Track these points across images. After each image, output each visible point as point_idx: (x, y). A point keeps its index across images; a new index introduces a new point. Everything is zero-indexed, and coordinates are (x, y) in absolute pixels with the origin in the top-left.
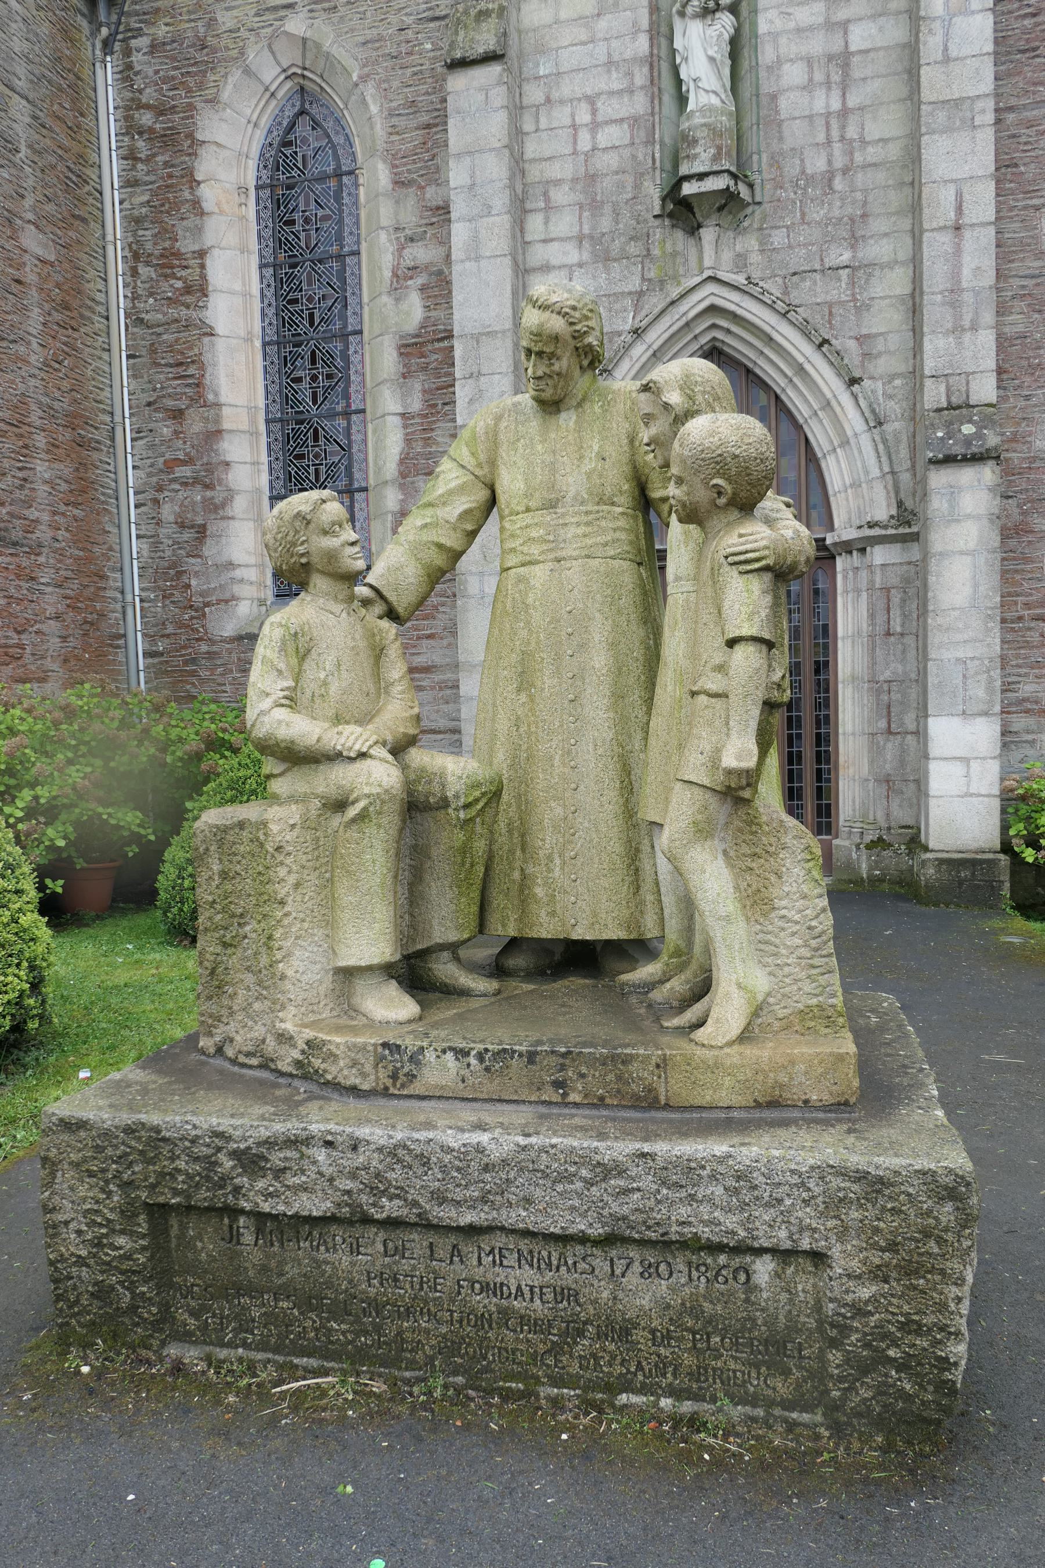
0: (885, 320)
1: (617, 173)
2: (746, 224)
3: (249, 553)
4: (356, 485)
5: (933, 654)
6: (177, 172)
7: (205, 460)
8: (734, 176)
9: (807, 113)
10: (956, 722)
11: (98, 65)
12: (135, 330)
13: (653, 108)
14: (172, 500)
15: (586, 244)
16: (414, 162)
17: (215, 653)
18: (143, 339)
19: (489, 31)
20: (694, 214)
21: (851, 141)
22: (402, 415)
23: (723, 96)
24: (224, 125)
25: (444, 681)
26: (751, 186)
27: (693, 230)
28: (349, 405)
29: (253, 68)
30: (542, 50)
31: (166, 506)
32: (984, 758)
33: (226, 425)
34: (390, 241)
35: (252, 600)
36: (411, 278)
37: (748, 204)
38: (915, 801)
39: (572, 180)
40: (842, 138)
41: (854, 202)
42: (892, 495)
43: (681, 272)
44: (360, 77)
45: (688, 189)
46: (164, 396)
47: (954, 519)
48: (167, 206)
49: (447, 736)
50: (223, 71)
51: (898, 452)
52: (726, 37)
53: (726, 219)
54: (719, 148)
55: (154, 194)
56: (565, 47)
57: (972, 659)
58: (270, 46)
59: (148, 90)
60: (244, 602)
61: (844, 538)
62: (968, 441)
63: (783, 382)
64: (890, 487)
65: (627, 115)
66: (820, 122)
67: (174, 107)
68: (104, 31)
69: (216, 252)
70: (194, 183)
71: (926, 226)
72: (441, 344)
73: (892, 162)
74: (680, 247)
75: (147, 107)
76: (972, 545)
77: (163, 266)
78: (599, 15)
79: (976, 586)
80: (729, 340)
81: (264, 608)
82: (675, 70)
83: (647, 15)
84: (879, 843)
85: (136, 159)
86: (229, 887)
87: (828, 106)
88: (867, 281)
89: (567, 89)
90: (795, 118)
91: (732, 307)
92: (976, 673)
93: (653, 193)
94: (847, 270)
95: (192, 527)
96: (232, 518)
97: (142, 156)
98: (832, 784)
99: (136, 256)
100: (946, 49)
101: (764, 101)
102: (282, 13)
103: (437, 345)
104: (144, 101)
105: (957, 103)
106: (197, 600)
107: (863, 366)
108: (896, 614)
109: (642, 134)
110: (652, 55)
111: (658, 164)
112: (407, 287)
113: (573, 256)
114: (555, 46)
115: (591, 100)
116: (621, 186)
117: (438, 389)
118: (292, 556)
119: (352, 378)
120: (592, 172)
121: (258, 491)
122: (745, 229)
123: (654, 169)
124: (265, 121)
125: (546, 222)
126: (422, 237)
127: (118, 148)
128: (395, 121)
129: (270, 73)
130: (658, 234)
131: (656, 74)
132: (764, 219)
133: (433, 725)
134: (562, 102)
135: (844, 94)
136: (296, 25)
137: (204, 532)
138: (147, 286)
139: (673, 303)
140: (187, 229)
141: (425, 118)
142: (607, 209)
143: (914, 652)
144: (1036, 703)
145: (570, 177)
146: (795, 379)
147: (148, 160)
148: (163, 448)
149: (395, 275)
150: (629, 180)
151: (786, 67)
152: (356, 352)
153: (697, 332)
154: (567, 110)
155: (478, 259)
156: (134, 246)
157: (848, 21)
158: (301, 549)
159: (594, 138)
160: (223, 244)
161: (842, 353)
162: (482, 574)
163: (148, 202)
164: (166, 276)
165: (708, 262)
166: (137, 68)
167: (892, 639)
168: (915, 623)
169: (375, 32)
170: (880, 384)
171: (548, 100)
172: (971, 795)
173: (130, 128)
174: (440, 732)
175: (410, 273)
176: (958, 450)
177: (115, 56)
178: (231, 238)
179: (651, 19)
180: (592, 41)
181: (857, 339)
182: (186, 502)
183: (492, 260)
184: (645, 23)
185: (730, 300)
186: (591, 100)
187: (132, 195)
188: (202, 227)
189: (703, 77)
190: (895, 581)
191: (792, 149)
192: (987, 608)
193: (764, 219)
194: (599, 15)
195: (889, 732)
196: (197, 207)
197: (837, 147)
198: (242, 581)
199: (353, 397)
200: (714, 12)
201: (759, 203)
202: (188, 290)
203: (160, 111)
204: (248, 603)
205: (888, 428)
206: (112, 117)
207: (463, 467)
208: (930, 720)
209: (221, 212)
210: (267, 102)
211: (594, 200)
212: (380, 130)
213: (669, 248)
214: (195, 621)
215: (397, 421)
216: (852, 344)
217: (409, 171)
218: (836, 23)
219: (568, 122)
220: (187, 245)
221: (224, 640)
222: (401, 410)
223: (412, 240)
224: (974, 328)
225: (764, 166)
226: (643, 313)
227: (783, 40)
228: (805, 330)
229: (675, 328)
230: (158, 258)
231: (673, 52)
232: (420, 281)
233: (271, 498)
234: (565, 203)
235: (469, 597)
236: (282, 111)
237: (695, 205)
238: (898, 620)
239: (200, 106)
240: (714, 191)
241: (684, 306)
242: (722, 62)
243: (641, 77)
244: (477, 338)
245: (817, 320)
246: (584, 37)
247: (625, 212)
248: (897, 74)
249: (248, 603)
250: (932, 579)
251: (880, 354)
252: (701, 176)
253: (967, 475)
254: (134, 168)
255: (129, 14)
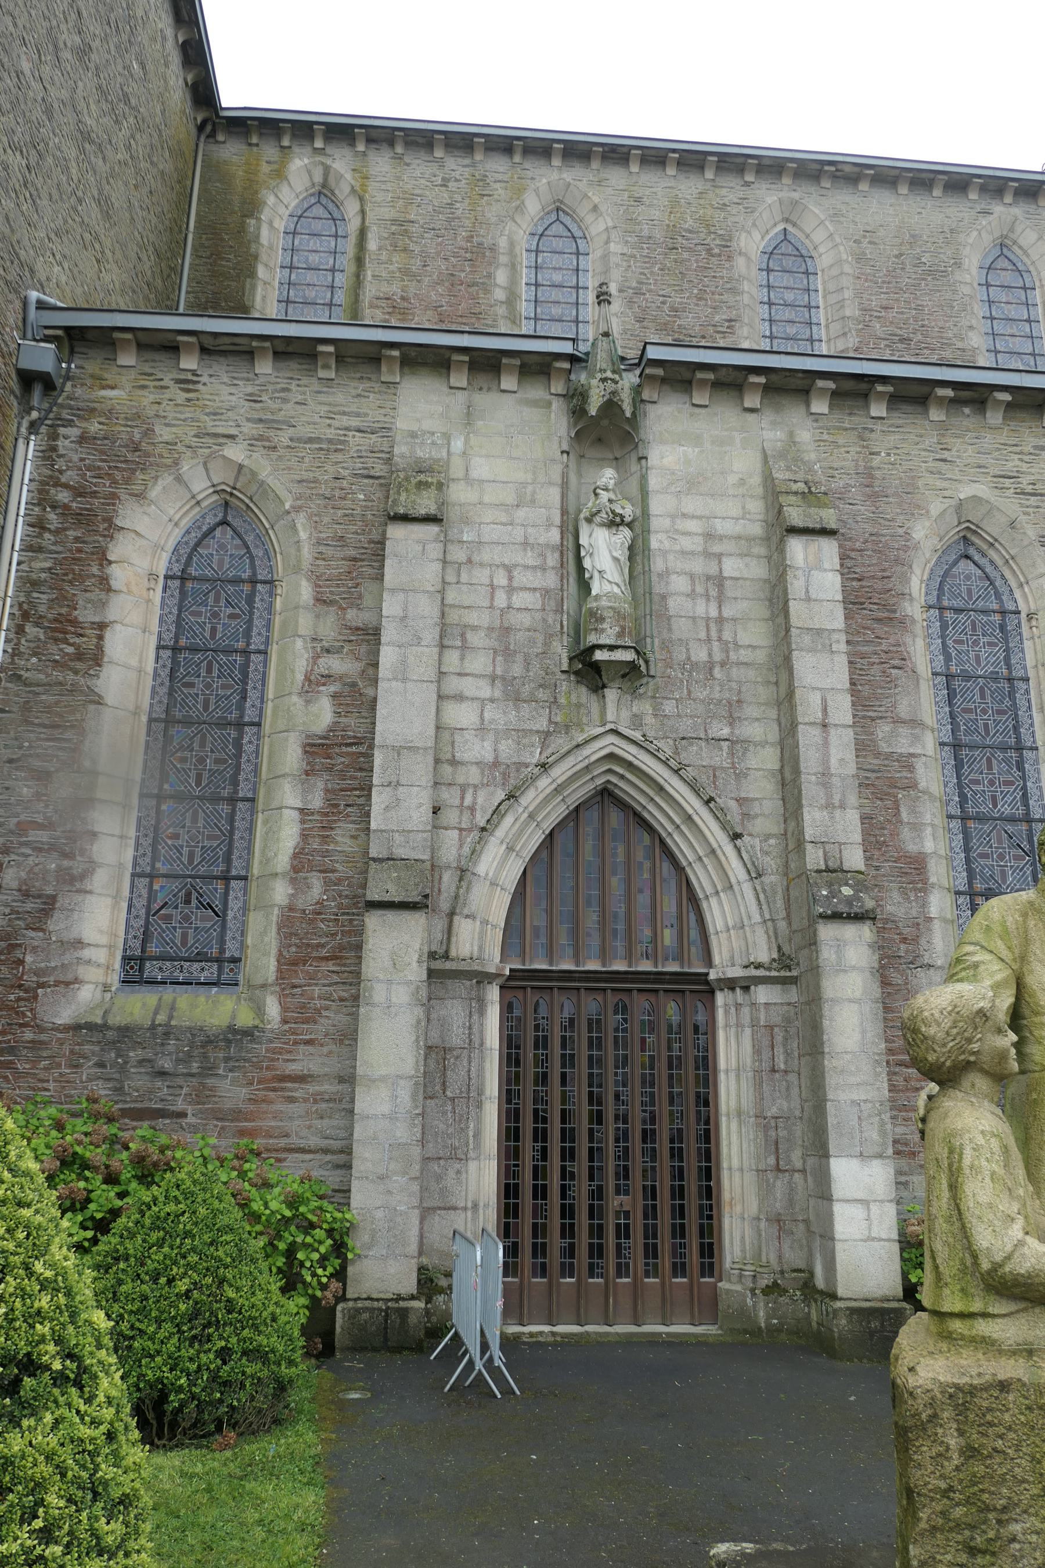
0: (761, 789)
1: (529, 630)
2: (641, 691)
3: (101, 932)
4: (234, 873)
5: (830, 1095)
6: (88, 548)
7: (68, 827)
8: (638, 652)
10: (854, 1164)
11: (21, 441)
12: (9, 685)
14: (19, 865)
16: (338, 586)
17: (41, 1042)
18: (18, 696)
19: (429, 498)
20: (600, 677)
21: (727, 643)
22: (301, 810)
24: (146, 518)
25: (320, 1093)
26: (647, 662)
27: (598, 688)
28: (236, 792)
29: (185, 478)
30: (466, 521)
31: (11, 871)
32: (882, 1201)
33: (100, 794)
34: (305, 648)
35: (97, 984)
36: (324, 685)
38: (804, 1242)
41: (730, 690)
42: (773, 939)
43: (585, 720)
44: (292, 507)
45: (599, 655)
46: (31, 756)
47: (842, 969)
48: (70, 576)
49: (318, 1156)
50: (153, 474)
51: (775, 902)
54: (623, 628)
55: (58, 562)
57: (865, 1101)
58: (205, 464)
59: (69, 473)
60: (87, 987)
61: (730, 975)
62: (849, 901)
63: (670, 828)
64: (771, 933)
66: (702, 624)
67: (95, 492)
68: (35, 415)
69: (118, 627)
70: (104, 560)
71: (800, 720)
72: (349, 749)
74: (584, 700)
75: (66, 486)
76: (858, 994)
77: (55, 630)
79: (863, 1032)
81: (108, 995)
82: (579, 560)
83: (559, 516)
84: (773, 1289)
85: (43, 528)
86: (980, 1469)
87: (707, 612)
88: (744, 754)
89: (486, 555)
91: (630, 758)
92: (870, 1116)
93: (561, 652)
95: (39, 896)
96: (90, 892)
97: (52, 527)
98: (715, 1222)
99: (25, 615)
100: (807, 591)
101: (656, 598)
102: (222, 440)
103: (344, 749)
104: (63, 480)
105: (819, 632)
106: (30, 980)
108: (779, 1050)
109: (553, 603)
112: (318, 692)
113: (486, 692)
115: (509, 569)
116: (532, 642)
117: (342, 790)
118: (963, 1053)
119: (243, 766)
121: (121, 866)
123: (562, 633)
124: (185, 523)
125: (462, 658)
126: (339, 650)
127: (26, 515)
128: (322, 548)
129: (200, 485)
132: (657, 689)
133: (302, 1143)
134: (481, 565)
136: (236, 453)
137: (53, 904)
138: (32, 645)
139: (578, 746)
140: (89, 601)
141: (352, 552)
142: (519, 658)
143: (797, 1090)
144: (906, 1145)
146: (682, 827)
147: (57, 532)
148: (19, 809)
149: (307, 679)
150: (540, 638)
151: (674, 577)
152: (250, 742)
154: (487, 572)
155: (404, 680)
156: (25, 606)
158: (975, 1047)
160: (127, 621)
162: (389, 982)
163: (50, 569)
164: (56, 640)
165: (610, 717)
166: (61, 451)
167: (777, 1075)
168: (796, 1061)
169: (311, 475)
170: (757, 841)
171: (470, 561)
172: (873, 1239)
173: (42, 498)
174: (310, 1152)
175: (323, 680)
176: (843, 908)
177: (40, 437)
178: (135, 617)
182: (36, 870)
184: (557, 520)
185: (629, 752)
186: (509, 569)
187: (32, 559)
188: (107, 601)
190: (777, 1020)
192: (875, 1054)
193: (657, 689)
195: (778, 1169)
196: (105, 584)
197: (716, 644)
198: (89, 962)
199: (242, 785)
202: (79, 656)
203: (79, 492)
204: (92, 987)
205: (767, 880)
206: (25, 488)
207: (1002, 960)
208: (832, 1161)
209: (129, 592)
210: (191, 508)
211: (507, 648)
212: (307, 553)
214: (22, 1003)
215: (295, 815)
216: (733, 804)
217: (331, 593)
219: (487, 581)
220: (86, 615)
221: (57, 1028)
222: (300, 806)
223: (328, 651)
224: (843, 806)
225: (656, 648)
226: (550, 751)
227: (671, 557)
228: (694, 787)
229: (575, 770)
230: (50, 622)
231: (578, 547)
232: (332, 689)
233: (133, 875)
235: (373, 1005)
236: (203, 517)
237: (603, 669)
238: (782, 1057)
239: (123, 497)
241: (587, 751)
244: (398, 750)
245: (703, 779)
246: (504, 520)
247: (536, 664)
249: (92, 987)
250: (826, 1023)
251: (756, 816)
252: (612, 648)
253: (850, 931)
254: (40, 536)
255: (62, 406)
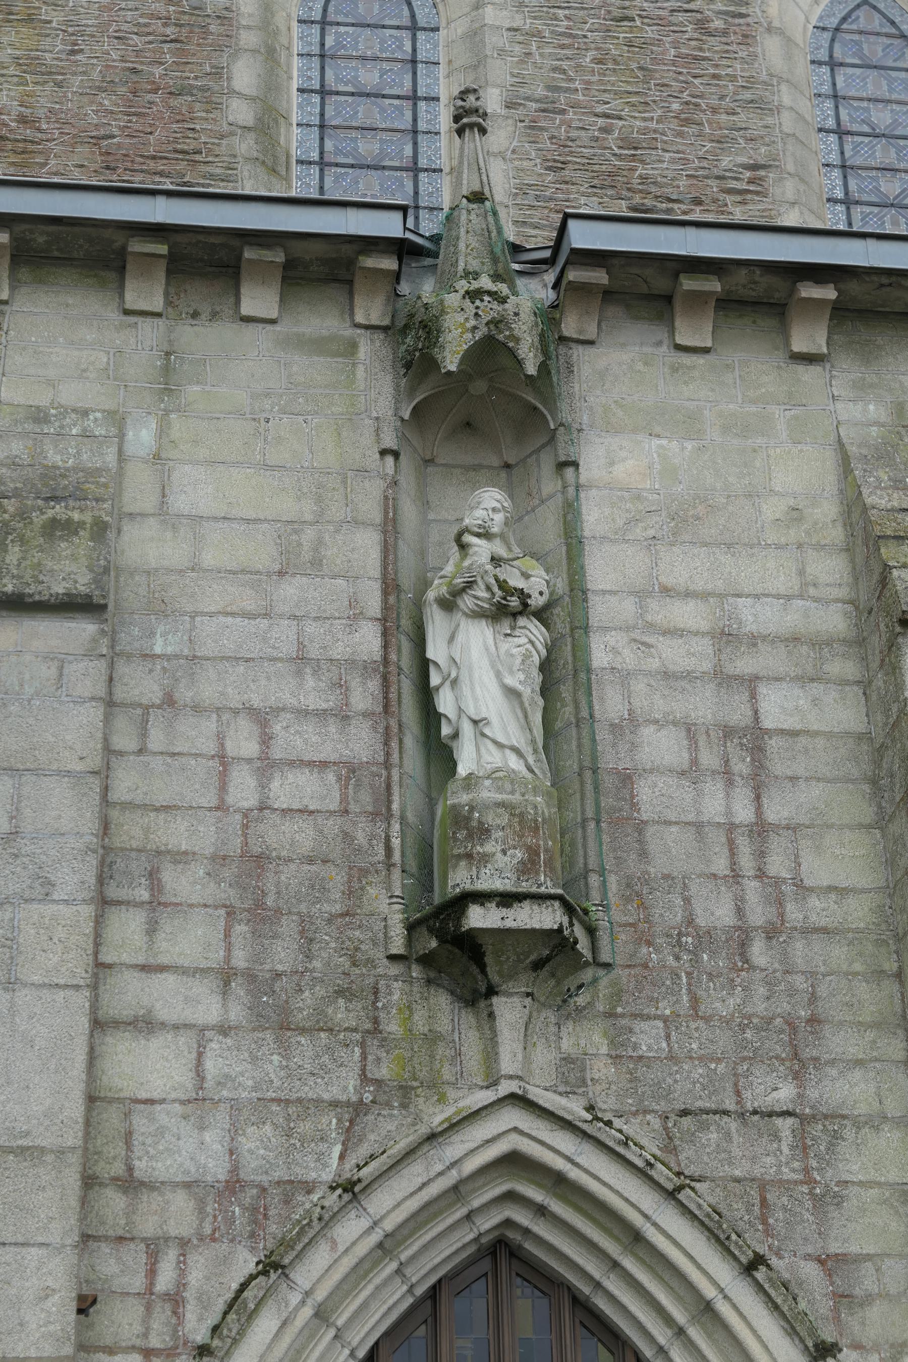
1: (311, 861)
8: (569, 909)
9: (691, 817)
13: (388, 754)
15: (238, 988)
19: (74, 558)
20: (483, 968)
21: (778, 882)
23: (531, 760)
26: (591, 931)
27: (477, 996)
30: (161, 608)
37: (587, 964)
39: (213, 858)
40: (761, 874)
41: (792, 992)
43: (447, 1073)
45: (478, 918)
52: (536, 660)
53: (545, 986)
54: (533, 852)
56: (211, 615)
63: (662, 1335)
65: (333, 757)
73: (857, 931)
74: (444, 1024)
78: (281, 573)
80: (541, 1229)
82: (426, 695)
87: (729, 812)
90: (669, 823)
93: (387, 911)
94: (790, 1121)
101: (608, 782)
107: (837, 1319)
109: (366, 797)
110: (386, 661)
111: (397, 857)
113: (208, 1008)
114: (189, 608)
115: (262, 719)
116: (319, 887)
120: (257, 850)
122: (579, 1010)
123: (389, 866)
125: (152, 929)
130: (397, 993)
131: (393, 696)
132: (617, 995)
134: (197, 709)
135: (758, 797)
139: (432, 1137)
142: (288, 926)
145: (208, 851)
146: (693, 1332)
150: (337, 879)
151: (647, 731)
153: (476, 1204)
154: (210, 725)
157: (756, 678)
159: (263, 787)
161: (793, 1286)
165: (508, 1063)
171: (169, 701)
179: (385, 601)
180: (266, 615)
181: (821, 1262)
183: (45, 993)
184: (373, 604)
185: (557, 1149)
186: (262, 719)
189: (495, 720)
191: (666, 877)
193: (617, 995)
194: (281, 573)
197: (752, 887)
200: (515, 615)
201: (607, 966)
211: (259, 904)
213: (420, 1023)
216: (811, 1271)
218: (736, 678)
219: (211, 747)
225: (613, 899)
226: (364, 1151)
231: (424, 665)
234: (195, 899)
237: (489, 949)
240: (534, 931)
241: (454, 1148)
242: (533, 702)
243: (364, 695)
246: (249, 605)
247: (327, 938)
248: (853, 781)
251: (868, 1300)
252: (507, 899)
